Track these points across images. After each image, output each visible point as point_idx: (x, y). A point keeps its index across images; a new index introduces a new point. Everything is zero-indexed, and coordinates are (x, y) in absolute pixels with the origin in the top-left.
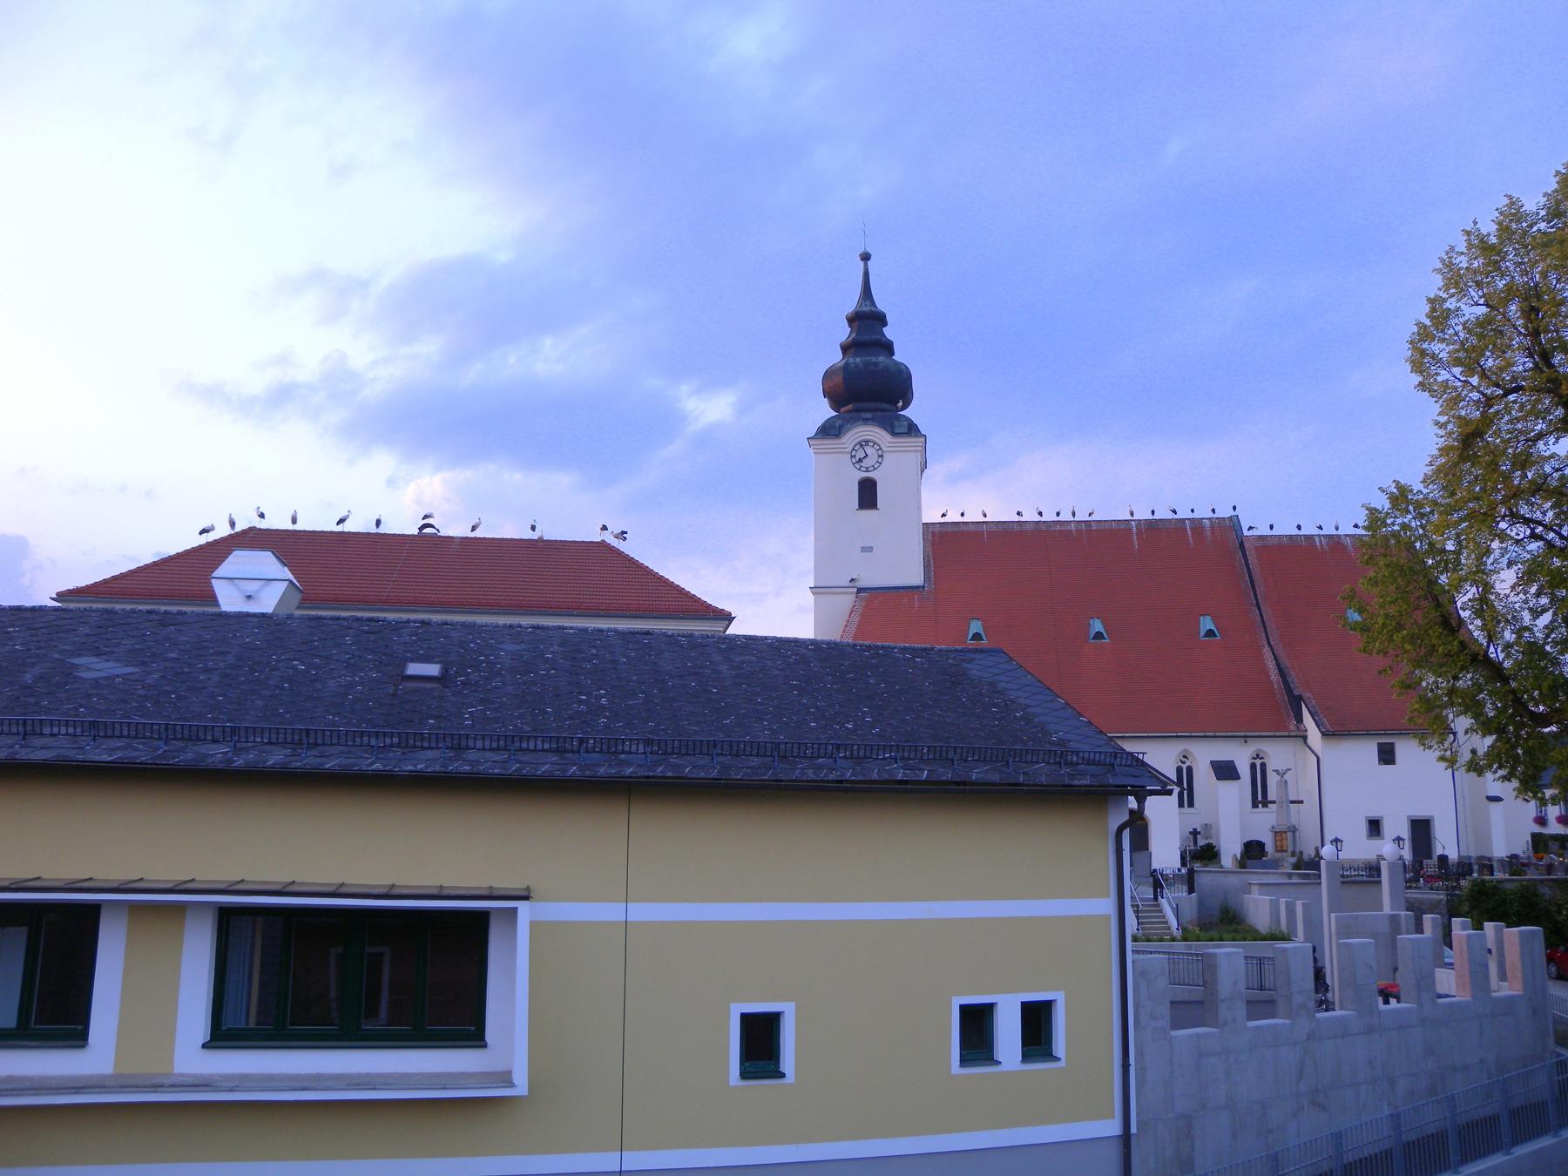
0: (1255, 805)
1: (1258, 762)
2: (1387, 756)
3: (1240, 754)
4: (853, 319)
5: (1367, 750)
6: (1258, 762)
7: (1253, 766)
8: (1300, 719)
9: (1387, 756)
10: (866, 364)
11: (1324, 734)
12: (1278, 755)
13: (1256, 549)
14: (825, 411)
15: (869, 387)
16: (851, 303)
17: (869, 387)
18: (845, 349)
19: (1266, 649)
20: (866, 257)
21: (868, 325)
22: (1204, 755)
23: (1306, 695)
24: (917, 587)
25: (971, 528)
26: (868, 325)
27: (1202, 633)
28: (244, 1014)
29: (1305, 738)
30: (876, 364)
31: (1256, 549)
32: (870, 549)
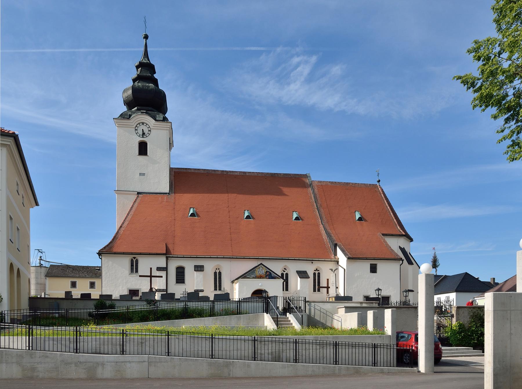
0: (314, 291)
1: (317, 272)
2: (373, 269)
3: (310, 268)
4: (141, 65)
5: (366, 266)
6: (317, 272)
7: (314, 274)
8: (335, 254)
9: (373, 269)
10: (143, 86)
11: (349, 258)
12: (325, 269)
13: (317, 186)
14: (124, 109)
15: (147, 99)
16: (139, 58)
17: (147, 99)
18: (134, 80)
19: (321, 226)
20: (146, 37)
21: (146, 70)
22: (293, 268)
23: (339, 243)
24: (166, 193)
25: (192, 171)
26: (146, 70)
27: (294, 218)
28: (479, 352)
29: (338, 262)
30: (149, 86)
31: (317, 186)
32: (144, 174)
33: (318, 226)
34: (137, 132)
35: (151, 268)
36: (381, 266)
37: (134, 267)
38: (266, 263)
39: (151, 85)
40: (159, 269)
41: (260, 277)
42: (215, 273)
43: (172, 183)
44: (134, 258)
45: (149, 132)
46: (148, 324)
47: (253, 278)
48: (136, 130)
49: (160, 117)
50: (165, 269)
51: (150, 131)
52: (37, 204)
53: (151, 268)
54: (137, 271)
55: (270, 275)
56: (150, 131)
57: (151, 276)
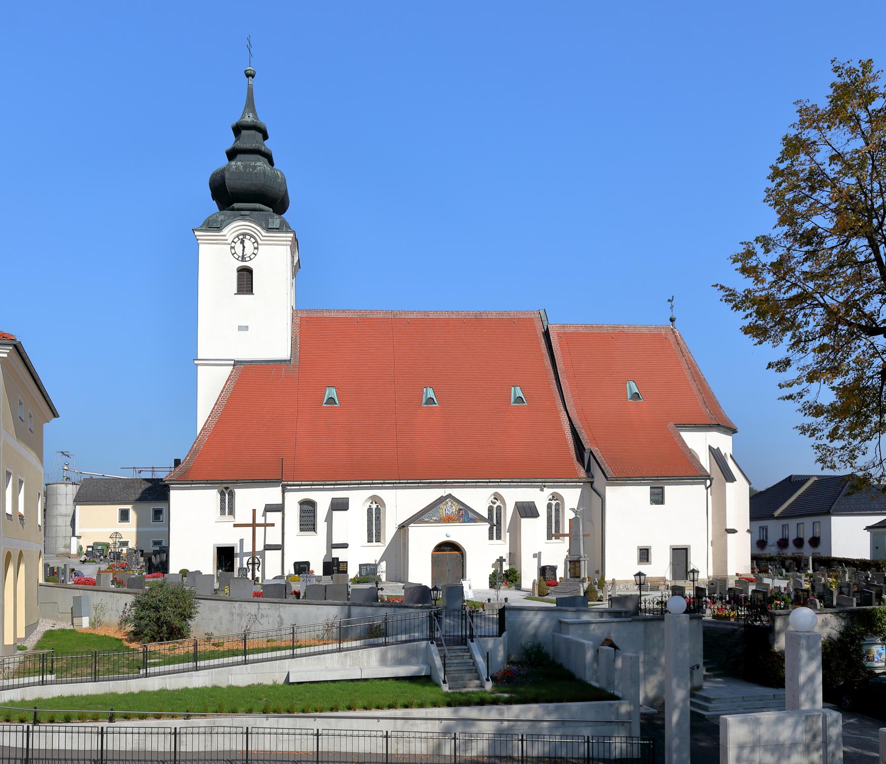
2: (658, 498)
5: (644, 492)
6: (554, 503)
7: (549, 506)
9: (658, 498)
32: (246, 328)
33: (558, 412)
34: (233, 251)
35: (254, 511)
36: (670, 491)
37: (228, 507)
38: (458, 493)
39: (261, 164)
40: (269, 508)
41: (448, 520)
42: (370, 510)
43: (296, 339)
44: (227, 488)
45: (255, 252)
46: (192, 676)
47: (436, 522)
48: (232, 248)
49: (276, 221)
50: (279, 508)
51: (256, 248)
52: (55, 415)
53: (254, 511)
54: (232, 512)
55: (466, 515)
56: (256, 248)
57: (254, 525)
